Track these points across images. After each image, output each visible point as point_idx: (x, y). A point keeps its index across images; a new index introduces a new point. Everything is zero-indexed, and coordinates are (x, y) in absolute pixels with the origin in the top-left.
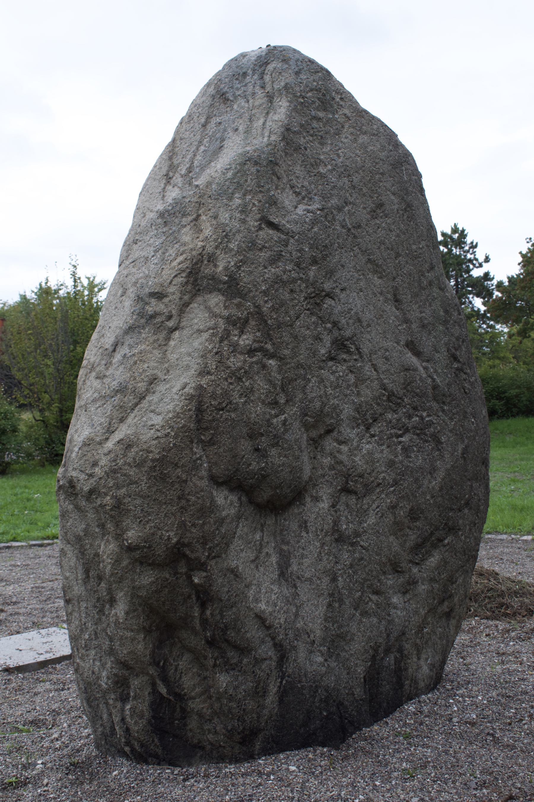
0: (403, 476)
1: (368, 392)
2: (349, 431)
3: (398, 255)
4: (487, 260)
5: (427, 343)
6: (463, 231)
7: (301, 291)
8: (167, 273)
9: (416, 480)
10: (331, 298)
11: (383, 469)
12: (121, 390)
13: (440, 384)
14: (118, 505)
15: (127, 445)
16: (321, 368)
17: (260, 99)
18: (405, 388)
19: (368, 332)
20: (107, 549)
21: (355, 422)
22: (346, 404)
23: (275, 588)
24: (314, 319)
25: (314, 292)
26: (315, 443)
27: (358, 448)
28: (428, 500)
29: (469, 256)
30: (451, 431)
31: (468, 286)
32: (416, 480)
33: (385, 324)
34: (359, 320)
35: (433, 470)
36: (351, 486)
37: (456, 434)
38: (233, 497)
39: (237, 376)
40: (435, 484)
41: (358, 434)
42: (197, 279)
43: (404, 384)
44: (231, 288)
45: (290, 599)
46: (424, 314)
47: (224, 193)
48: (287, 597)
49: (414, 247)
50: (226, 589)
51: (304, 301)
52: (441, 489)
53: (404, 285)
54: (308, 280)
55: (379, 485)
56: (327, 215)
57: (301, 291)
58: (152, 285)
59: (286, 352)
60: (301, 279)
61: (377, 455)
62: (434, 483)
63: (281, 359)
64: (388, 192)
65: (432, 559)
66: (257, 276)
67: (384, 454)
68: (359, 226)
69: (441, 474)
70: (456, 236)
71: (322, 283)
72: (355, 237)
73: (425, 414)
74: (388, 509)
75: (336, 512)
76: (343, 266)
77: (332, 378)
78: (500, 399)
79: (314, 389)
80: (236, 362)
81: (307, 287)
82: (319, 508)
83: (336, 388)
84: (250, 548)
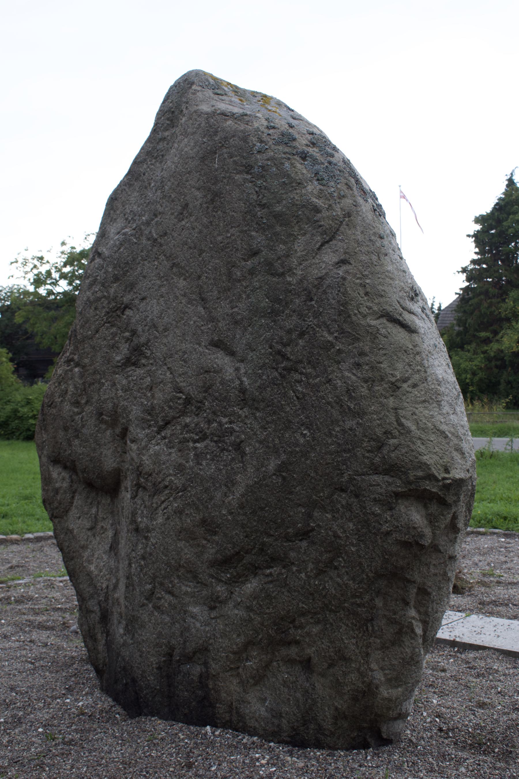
0: (192, 483)
1: (160, 395)
2: (139, 431)
3: (201, 252)
7: (104, 307)
9: (206, 490)
10: (130, 308)
11: (171, 472)
13: (248, 387)
16: (115, 373)
18: (206, 391)
19: (166, 336)
21: (145, 423)
22: (135, 405)
23: (105, 557)
24: (114, 329)
25: (116, 306)
27: (146, 447)
28: (224, 515)
30: (261, 442)
32: (207, 490)
33: (185, 325)
34: (155, 326)
35: (230, 483)
37: (268, 447)
38: (65, 474)
40: (234, 498)
41: (147, 435)
43: (204, 387)
45: (114, 571)
46: (236, 310)
48: (111, 568)
49: (219, 238)
50: (67, 544)
51: (105, 315)
52: (242, 506)
53: (210, 282)
54: (109, 297)
55: (166, 487)
57: (104, 307)
59: (87, 361)
60: (104, 297)
61: (163, 458)
62: (231, 498)
63: (83, 367)
64: (193, 190)
65: (249, 585)
68: (166, 234)
69: (239, 490)
71: (122, 297)
72: (161, 245)
73: (224, 420)
74: (175, 512)
75: (134, 504)
76: (145, 277)
77: (124, 382)
81: (109, 303)
83: (126, 390)
84: (86, 518)
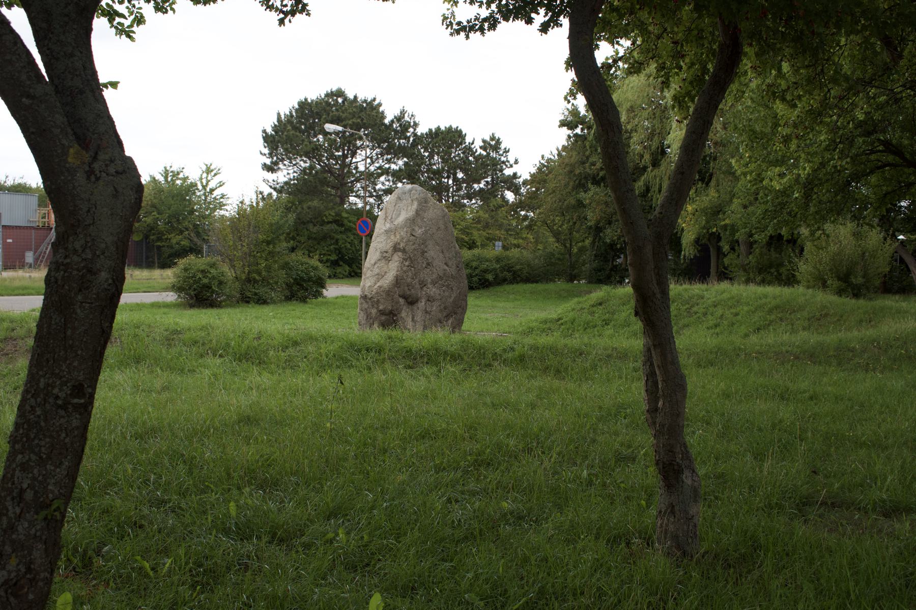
4: (516, 162)
5: (450, 264)
6: (499, 139)
8: (388, 247)
12: (378, 274)
14: (378, 301)
15: (380, 287)
17: (410, 201)
20: (374, 311)
26: (421, 288)
29: (503, 159)
31: (501, 182)
36: (430, 299)
39: (405, 272)
42: (396, 249)
44: (404, 251)
47: (402, 227)
56: (426, 231)
58: (385, 249)
66: (410, 248)
67: (438, 292)
70: (493, 143)
78: (509, 271)
79: (422, 275)
80: (405, 268)
82: (422, 304)
